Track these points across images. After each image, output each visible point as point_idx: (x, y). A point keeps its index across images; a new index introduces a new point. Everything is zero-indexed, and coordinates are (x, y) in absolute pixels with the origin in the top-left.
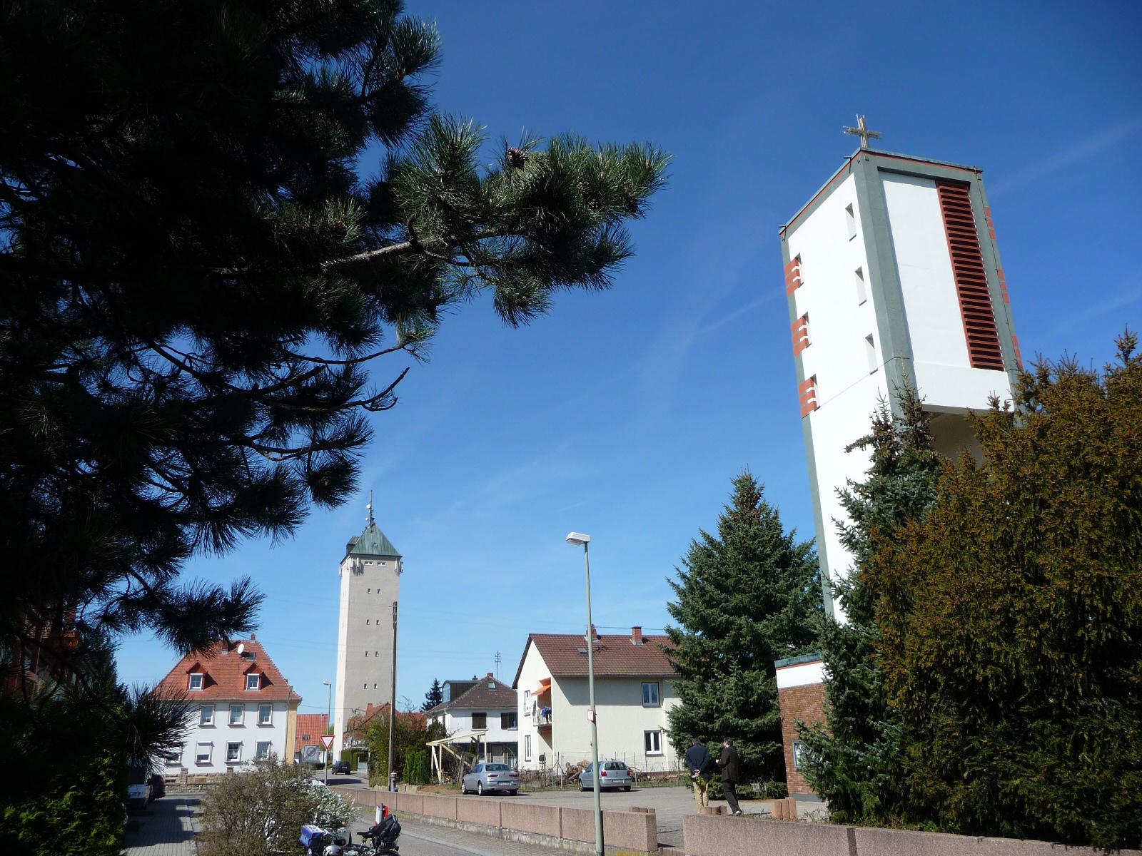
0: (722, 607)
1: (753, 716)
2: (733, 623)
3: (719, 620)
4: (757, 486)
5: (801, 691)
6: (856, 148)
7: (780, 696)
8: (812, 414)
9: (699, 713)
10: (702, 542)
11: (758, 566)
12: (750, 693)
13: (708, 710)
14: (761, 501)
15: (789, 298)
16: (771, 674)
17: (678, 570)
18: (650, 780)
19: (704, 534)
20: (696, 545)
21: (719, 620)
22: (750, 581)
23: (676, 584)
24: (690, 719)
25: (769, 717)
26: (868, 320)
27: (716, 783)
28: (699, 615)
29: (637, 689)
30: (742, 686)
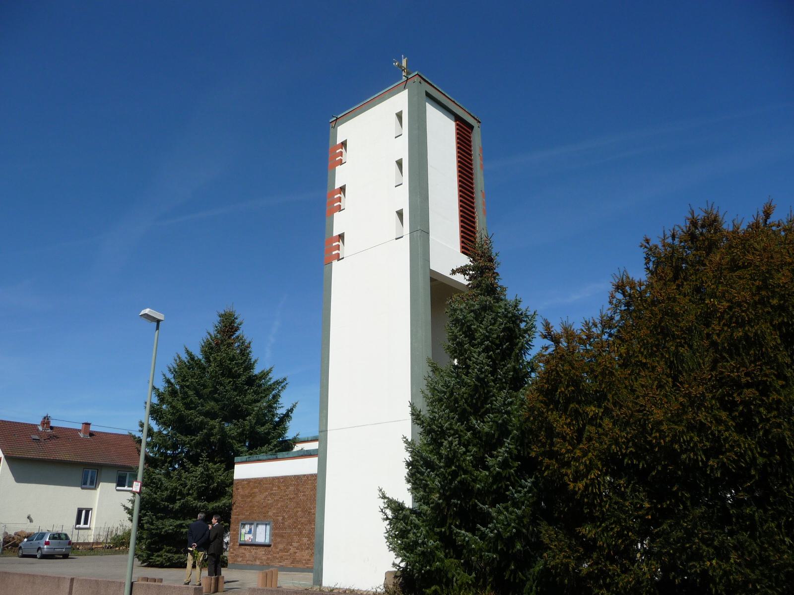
0: (198, 410)
1: (209, 500)
2: (207, 423)
3: (196, 420)
4: (237, 321)
5: (305, 478)
6: (414, 72)
7: (234, 486)
8: (335, 263)
9: (163, 495)
10: (185, 357)
11: (231, 381)
12: (211, 481)
13: (171, 492)
14: (237, 333)
15: (329, 173)
16: (230, 467)
17: (164, 375)
18: (78, 549)
19: (187, 352)
20: (179, 358)
21: (196, 420)
22: (224, 392)
23: (157, 387)
24: (154, 499)
25: (224, 502)
26: (402, 199)
27: (165, 553)
28: (178, 414)
29: (78, 474)
30: (207, 475)
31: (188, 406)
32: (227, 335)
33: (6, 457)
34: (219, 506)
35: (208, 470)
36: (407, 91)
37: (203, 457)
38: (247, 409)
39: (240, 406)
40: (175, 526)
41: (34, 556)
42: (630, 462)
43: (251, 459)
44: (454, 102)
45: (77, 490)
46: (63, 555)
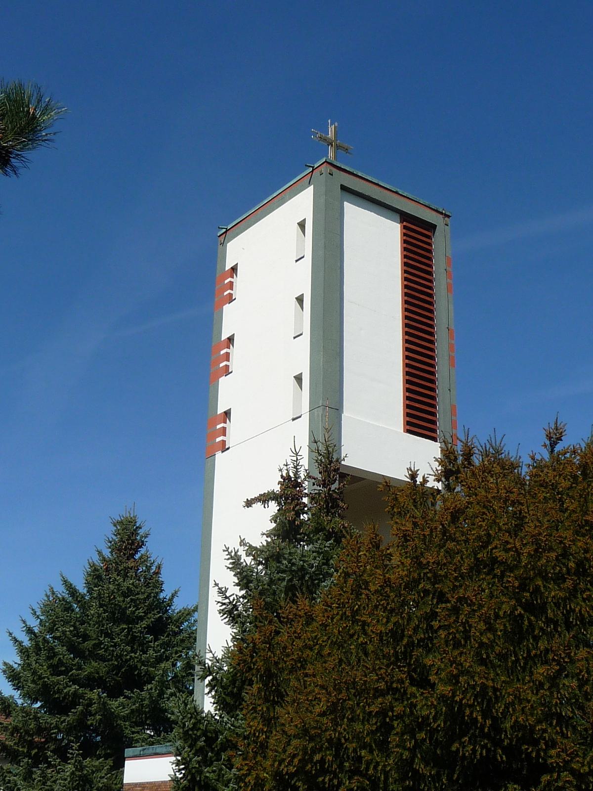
3: (65, 691)
4: (141, 532)
5: (151, 788)
8: (219, 455)
10: (61, 591)
14: (143, 551)
16: (119, 765)
17: (24, 622)
19: (66, 582)
20: (53, 593)
22: (111, 646)
28: (41, 682)
30: (80, 776)
31: (56, 670)
32: (124, 554)
35: (82, 769)
36: (312, 187)
37: (73, 750)
38: (147, 672)
39: (136, 667)
44: (396, 193)
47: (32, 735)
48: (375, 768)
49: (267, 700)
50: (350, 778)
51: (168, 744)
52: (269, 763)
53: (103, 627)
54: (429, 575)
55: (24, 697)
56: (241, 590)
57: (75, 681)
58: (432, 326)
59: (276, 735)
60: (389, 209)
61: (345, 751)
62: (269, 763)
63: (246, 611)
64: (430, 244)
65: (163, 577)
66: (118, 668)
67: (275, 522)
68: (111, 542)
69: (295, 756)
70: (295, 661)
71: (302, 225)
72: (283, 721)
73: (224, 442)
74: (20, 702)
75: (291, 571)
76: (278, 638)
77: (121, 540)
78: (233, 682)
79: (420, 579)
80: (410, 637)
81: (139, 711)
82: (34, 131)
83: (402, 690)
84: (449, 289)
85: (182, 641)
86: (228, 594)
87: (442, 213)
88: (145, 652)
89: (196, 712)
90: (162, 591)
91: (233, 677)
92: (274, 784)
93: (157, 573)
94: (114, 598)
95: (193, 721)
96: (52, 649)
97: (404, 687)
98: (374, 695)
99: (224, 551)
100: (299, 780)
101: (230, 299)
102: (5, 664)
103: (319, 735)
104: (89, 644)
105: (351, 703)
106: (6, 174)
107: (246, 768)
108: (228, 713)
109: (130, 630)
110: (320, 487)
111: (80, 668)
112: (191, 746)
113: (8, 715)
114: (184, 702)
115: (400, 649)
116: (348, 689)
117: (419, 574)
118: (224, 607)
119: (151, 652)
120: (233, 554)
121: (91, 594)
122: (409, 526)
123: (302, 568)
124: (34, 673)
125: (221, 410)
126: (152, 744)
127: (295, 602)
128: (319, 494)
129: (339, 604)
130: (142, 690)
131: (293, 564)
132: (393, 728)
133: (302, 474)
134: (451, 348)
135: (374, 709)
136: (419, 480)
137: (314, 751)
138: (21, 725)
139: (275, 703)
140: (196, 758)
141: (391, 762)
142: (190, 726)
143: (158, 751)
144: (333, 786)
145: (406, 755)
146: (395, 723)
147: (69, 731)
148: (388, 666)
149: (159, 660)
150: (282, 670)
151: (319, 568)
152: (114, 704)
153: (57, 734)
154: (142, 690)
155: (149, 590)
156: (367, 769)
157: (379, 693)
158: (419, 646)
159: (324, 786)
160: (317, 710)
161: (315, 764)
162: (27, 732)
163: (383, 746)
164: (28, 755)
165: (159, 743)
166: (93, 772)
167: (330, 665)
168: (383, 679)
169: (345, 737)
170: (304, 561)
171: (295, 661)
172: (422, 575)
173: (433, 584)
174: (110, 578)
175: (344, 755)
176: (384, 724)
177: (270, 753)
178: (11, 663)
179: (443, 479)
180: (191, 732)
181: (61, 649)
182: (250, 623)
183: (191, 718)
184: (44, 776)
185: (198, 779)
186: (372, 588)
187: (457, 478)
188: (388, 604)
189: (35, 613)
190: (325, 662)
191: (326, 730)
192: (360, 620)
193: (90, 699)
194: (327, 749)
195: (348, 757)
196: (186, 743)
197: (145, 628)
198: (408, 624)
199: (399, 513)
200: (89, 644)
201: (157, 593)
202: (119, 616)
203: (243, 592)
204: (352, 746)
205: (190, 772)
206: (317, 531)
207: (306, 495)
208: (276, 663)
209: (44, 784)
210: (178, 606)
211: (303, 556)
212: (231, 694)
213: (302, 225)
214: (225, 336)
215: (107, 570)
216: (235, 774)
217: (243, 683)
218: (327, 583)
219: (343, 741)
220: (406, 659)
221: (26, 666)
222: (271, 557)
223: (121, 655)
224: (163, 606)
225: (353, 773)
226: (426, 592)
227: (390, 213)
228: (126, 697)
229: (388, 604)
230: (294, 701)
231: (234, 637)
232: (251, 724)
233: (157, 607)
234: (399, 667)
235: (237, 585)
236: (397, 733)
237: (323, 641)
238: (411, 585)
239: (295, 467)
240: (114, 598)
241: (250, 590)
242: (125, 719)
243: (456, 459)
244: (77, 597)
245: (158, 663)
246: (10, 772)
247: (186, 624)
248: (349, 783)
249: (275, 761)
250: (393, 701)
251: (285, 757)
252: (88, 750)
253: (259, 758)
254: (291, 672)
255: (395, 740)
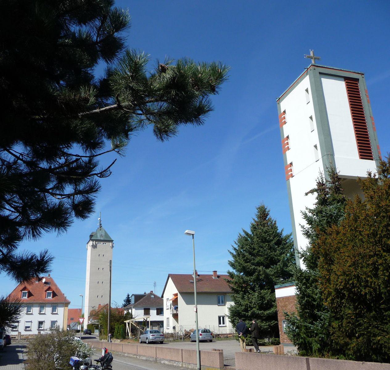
1: (265, 310)
4: (267, 210)
5: (286, 299)
7: (277, 301)
8: (291, 179)
10: (243, 234)
13: (246, 307)
14: (268, 217)
16: (273, 291)
18: (221, 337)
19: (244, 231)
20: (241, 235)
25: (272, 310)
26: (315, 138)
29: (215, 298)
30: (260, 296)
31: (246, 261)
33: (179, 292)
34: (270, 313)
38: (277, 259)
40: (250, 324)
41: (145, 343)
42: (68, 329)
43: (282, 286)
44: (341, 70)
45: (216, 307)
46: (210, 340)
47: (242, 284)
48: (374, 284)
49: (327, 263)
50: (365, 289)
51: (289, 283)
52: (332, 286)
53: (259, 244)
54: (384, 210)
55: (237, 271)
56: (309, 225)
57: (253, 264)
58: (364, 117)
59: (333, 275)
60: (337, 76)
61: (361, 279)
62: (332, 286)
63: (312, 233)
64: (358, 87)
65: (277, 225)
66: (267, 258)
67: (318, 199)
68: (257, 215)
69: (342, 282)
70: (336, 248)
71: (307, 90)
72: (335, 270)
73: (292, 174)
74: (236, 273)
75: (327, 216)
76: (327, 241)
77: (261, 214)
78: (312, 259)
79: (380, 212)
80: (380, 234)
81: (277, 272)
82: (222, 77)
83: (380, 254)
84: (368, 101)
85: (288, 246)
86: (305, 227)
87: (360, 74)
88: (276, 252)
89: (300, 270)
90: (278, 230)
91: (312, 256)
92: (335, 293)
93: (275, 224)
94: (262, 234)
95: (300, 273)
96: (243, 254)
97: (381, 253)
98: (369, 257)
99: (301, 212)
100: (344, 291)
101: (285, 123)
102: (229, 261)
103: (350, 274)
104: (255, 251)
105: (360, 261)
106: (214, 94)
107: (324, 288)
108: (312, 270)
109: (269, 245)
110: (332, 184)
111: (254, 260)
112: (301, 282)
113: (233, 278)
114: (295, 267)
115: (377, 239)
116: (358, 256)
117: (380, 210)
118: (304, 232)
119: (278, 251)
120: (304, 213)
121: (253, 234)
122: (372, 193)
123: (331, 215)
124: (239, 263)
125: (289, 163)
126: (284, 283)
127: (331, 227)
128: (332, 187)
129: (349, 226)
130: (277, 265)
131: (327, 214)
132: (379, 269)
133: (325, 181)
134: (373, 124)
135: (370, 262)
136: (372, 175)
137: (349, 280)
138: (237, 281)
139: (330, 264)
140: (303, 286)
141: (380, 281)
142: (299, 275)
143: (286, 285)
144: (359, 292)
145: (386, 278)
146: (380, 267)
147: (254, 281)
148: (373, 246)
149: (281, 254)
150: (331, 252)
151: (337, 214)
152: (268, 271)
153: (250, 283)
154: (277, 265)
155: (273, 230)
156: (371, 285)
157: (371, 256)
158: (384, 237)
159: (355, 292)
160: (348, 265)
161: (350, 284)
162: (240, 283)
163: (376, 276)
164: (242, 291)
165: (286, 282)
166: (265, 295)
167: (349, 248)
168: (372, 251)
169: (360, 274)
170: (331, 212)
171: (336, 248)
172: (381, 210)
173: (386, 213)
174: (259, 228)
175: (361, 280)
176: (375, 267)
177: (332, 282)
178: (231, 261)
179: (382, 174)
180: (300, 278)
181: (246, 254)
182: (315, 237)
183: (299, 272)
184: (248, 297)
185: (305, 293)
186: (361, 218)
187: (388, 172)
188: (369, 223)
189: (236, 243)
190: (347, 247)
191: (353, 272)
192: (358, 230)
193: (260, 270)
194: (354, 279)
195: (363, 281)
196: (299, 281)
197: (274, 243)
198: (378, 229)
199: (367, 189)
200: (255, 251)
201: (276, 231)
202: (264, 240)
203: (310, 226)
204: (363, 277)
205: (302, 292)
206: (334, 200)
207: (327, 188)
208: (328, 250)
209: (249, 300)
210: (284, 234)
211: (330, 210)
212: (312, 263)
213: (307, 90)
214: (285, 136)
215: (257, 225)
216: (319, 291)
217: (316, 258)
218: (341, 218)
219: (360, 275)
220: (380, 243)
221: (236, 261)
222: (319, 212)
223: (267, 254)
224: (279, 235)
225: (365, 287)
226: (384, 217)
227: (340, 78)
228: (271, 268)
229: (369, 223)
230: (338, 263)
231: (310, 243)
232: (322, 272)
233: (277, 235)
234: (377, 246)
235: (308, 224)
236: (381, 271)
237: (345, 240)
238: (377, 215)
239: (322, 178)
240: (262, 234)
241: (313, 225)
242: (273, 275)
243: (386, 165)
244: (249, 236)
245: (281, 255)
246: (237, 297)
247: (288, 240)
248: (365, 290)
249: (334, 285)
250: (377, 259)
251: (338, 283)
252: (262, 287)
253: (327, 284)
254: (334, 252)
255: (380, 273)
